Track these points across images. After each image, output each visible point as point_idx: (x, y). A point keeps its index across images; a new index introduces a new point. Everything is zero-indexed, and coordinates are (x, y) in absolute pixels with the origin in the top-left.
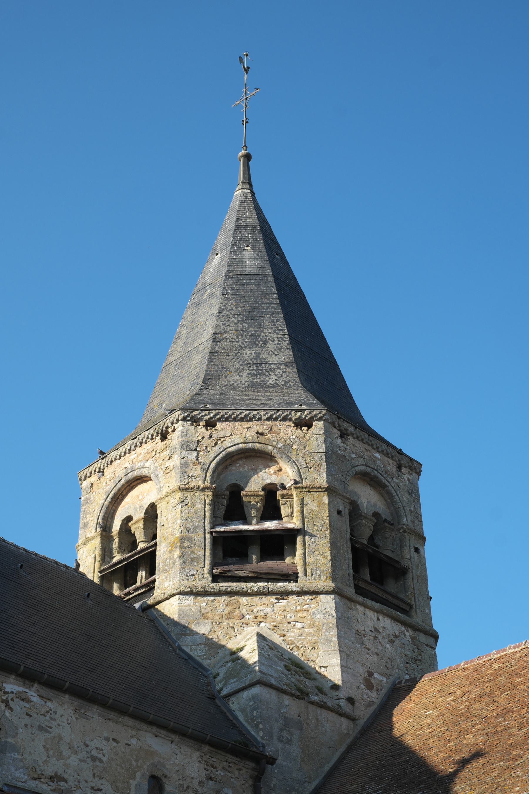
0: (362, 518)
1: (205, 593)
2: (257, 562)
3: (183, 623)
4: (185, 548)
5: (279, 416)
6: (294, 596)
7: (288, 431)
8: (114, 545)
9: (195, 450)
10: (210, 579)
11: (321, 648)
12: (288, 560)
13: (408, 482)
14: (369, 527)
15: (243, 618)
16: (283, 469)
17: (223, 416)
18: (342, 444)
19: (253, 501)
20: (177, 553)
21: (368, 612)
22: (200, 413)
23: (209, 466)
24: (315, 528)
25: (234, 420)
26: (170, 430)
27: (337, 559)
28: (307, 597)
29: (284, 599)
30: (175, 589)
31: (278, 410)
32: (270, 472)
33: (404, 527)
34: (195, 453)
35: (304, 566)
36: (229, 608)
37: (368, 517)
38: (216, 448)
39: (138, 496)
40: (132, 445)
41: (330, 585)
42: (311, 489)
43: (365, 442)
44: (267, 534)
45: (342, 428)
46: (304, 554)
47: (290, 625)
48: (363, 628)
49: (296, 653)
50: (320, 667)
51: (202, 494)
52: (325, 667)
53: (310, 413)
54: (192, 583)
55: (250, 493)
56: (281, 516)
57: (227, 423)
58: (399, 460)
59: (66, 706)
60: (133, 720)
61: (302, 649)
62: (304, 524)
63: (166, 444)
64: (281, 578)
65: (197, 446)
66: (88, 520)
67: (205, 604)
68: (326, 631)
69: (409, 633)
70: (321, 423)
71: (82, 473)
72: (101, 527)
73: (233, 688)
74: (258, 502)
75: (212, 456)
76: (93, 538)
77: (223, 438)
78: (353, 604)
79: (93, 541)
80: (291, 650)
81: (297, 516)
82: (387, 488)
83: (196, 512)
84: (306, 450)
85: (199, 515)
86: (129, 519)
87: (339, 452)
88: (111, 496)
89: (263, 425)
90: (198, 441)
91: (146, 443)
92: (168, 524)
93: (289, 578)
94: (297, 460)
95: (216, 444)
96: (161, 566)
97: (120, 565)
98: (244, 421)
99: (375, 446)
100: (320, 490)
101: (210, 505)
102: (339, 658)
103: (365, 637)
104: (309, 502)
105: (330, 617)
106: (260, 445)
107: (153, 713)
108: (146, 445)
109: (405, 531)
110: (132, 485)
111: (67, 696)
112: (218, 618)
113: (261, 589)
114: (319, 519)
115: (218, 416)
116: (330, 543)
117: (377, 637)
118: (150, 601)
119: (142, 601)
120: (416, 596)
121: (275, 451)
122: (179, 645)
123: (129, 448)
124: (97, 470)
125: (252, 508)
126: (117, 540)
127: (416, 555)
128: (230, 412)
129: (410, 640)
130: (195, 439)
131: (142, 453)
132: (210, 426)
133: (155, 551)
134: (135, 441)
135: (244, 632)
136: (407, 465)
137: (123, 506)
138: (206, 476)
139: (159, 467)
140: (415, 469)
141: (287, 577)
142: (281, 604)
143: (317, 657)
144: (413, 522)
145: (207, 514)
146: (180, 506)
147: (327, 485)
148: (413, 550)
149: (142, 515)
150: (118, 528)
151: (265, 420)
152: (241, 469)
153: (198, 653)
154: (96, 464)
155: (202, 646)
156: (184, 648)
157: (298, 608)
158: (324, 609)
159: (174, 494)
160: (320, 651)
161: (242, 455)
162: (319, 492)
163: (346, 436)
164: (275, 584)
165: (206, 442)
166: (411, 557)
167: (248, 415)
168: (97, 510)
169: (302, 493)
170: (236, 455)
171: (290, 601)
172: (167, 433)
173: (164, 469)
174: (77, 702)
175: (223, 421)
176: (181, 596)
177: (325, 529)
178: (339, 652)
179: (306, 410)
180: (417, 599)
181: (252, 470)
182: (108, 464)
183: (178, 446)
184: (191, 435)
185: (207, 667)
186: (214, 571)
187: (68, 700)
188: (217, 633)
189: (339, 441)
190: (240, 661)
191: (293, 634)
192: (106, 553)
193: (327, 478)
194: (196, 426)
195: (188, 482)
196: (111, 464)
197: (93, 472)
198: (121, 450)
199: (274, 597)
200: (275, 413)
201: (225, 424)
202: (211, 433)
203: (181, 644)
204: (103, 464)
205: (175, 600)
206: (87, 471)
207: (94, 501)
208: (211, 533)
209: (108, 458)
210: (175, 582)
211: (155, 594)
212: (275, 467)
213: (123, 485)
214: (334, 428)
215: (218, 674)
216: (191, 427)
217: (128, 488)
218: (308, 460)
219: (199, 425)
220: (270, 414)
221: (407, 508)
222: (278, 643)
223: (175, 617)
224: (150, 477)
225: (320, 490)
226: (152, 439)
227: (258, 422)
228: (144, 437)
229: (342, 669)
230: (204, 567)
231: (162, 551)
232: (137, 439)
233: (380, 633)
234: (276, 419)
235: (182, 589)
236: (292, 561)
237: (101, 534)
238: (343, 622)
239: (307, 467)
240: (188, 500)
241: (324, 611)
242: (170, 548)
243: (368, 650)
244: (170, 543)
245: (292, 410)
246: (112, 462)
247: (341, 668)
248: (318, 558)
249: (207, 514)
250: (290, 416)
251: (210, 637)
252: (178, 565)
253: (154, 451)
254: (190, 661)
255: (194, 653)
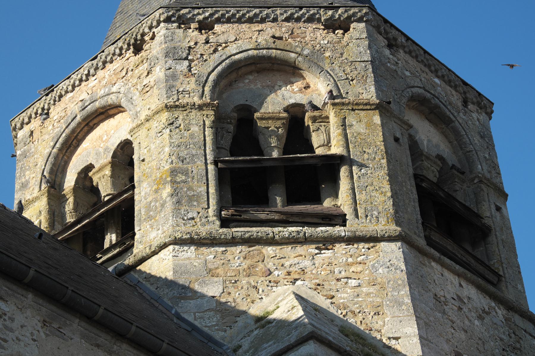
0: (424, 158)
1: (211, 242)
2: (283, 206)
3: (181, 283)
4: (179, 183)
5: (303, 15)
6: (342, 244)
7: (315, 35)
8: (66, 207)
9: (186, 59)
10: (218, 223)
11: (389, 313)
12: (328, 203)
13: (478, 123)
14: (433, 172)
15: (269, 275)
16: (312, 86)
17: (223, 15)
18: (391, 57)
19: (272, 125)
20: (168, 190)
21: (446, 273)
22: (190, 12)
23: (208, 78)
24: (366, 156)
25: (239, 21)
26: (147, 38)
27: (400, 197)
28: (361, 245)
29: (328, 249)
30: (165, 244)
31: (301, 8)
32: (293, 90)
33: (480, 175)
34: (186, 63)
35: (353, 206)
36: (249, 262)
37: (431, 158)
38: (217, 55)
39: (101, 137)
40: (90, 68)
41: (393, 229)
42: (357, 106)
43: (420, 60)
44: (297, 163)
45: (390, 36)
46: (353, 189)
47: (339, 283)
48: (442, 293)
49: (352, 320)
50: (389, 338)
51: (199, 114)
52: (397, 339)
53: (346, 11)
54: (192, 229)
55: (267, 116)
56: (312, 147)
57: (229, 25)
58: (465, 93)
59: (29, 313)
60: (135, 352)
61: (360, 314)
62: (349, 151)
63: (141, 57)
64: (320, 221)
65: (189, 54)
66: (27, 178)
67: (212, 256)
68: (394, 289)
69: (501, 312)
70: (362, 25)
71: (17, 119)
72: (48, 182)
73: (270, 352)
74: (280, 127)
75: (210, 66)
76: (37, 198)
77: (226, 43)
78: (426, 259)
79: (36, 204)
80: (344, 316)
81: (338, 141)
82: (453, 124)
83: (192, 136)
84: (343, 58)
85: (196, 140)
86: (90, 167)
87: (389, 65)
88: (61, 140)
89: (281, 27)
90: (190, 47)
91: (111, 62)
92: (151, 156)
93: (333, 222)
94: (333, 70)
95: (215, 51)
96: (143, 213)
97: (79, 226)
98: (253, 23)
99: (433, 68)
100: (368, 107)
101: (212, 128)
102: (416, 326)
103: (446, 305)
104: (354, 123)
105: (398, 272)
106: (279, 52)
107: (167, 341)
108: (112, 65)
109: (481, 181)
110: (91, 124)
111: (30, 296)
112: (233, 274)
113: (294, 234)
114: (369, 145)
115: (216, 16)
116: (389, 175)
117: (461, 309)
118: (129, 260)
119: (116, 265)
120: (504, 265)
121: (300, 59)
122: (176, 311)
123: (86, 72)
124: (40, 111)
125: (270, 136)
126: (71, 200)
127: (498, 214)
128: (233, 11)
129: (503, 320)
130: (186, 45)
131: (107, 76)
132: (205, 30)
133: (131, 201)
134: (95, 62)
135: (273, 293)
136: (475, 100)
137: (79, 154)
138: (203, 91)
139: (132, 88)
140: (485, 107)
141: (330, 220)
142: (324, 255)
143: (384, 326)
144: (490, 172)
145: (207, 139)
146: (168, 130)
147: (378, 101)
148: (493, 207)
149: (109, 159)
150: (73, 184)
151: (283, 21)
152: (252, 86)
153: (207, 323)
154: (37, 105)
155: (212, 313)
156: (185, 316)
157: (350, 260)
158: (388, 260)
159: (158, 116)
160: (387, 317)
161: (253, 68)
162: (367, 110)
163: (395, 48)
164: (313, 229)
165: (200, 49)
166: (492, 216)
167: (259, 15)
168: (41, 163)
169: (343, 111)
170: (245, 66)
171: (338, 251)
172: (143, 41)
173: (140, 88)
174: (47, 308)
175: (223, 23)
176: (177, 247)
177: (380, 157)
178: (415, 318)
179: (339, 7)
180: (505, 269)
181: (268, 86)
182: (55, 101)
183: (160, 56)
184: (178, 39)
185: (222, 341)
186: (223, 213)
187: (32, 303)
188: (232, 295)
189: (387, 52)
190: (274, 324)
191: (346, 295)
192: (56, 218)
193: (377, 92)
194: (186, 29)
195: (178, 99)
196: (60, 100)
197: (33, 116)
198: (75, 77)
199: (314, 246)
200: (296, 12)
201: (226, 26)
202: (208, 38)
203: (179, 310)
204: (47, 102)
205: (168, 253)
206: (25, 116)
207: (35, 153)
208: (216, 163)
209: (55, 92)
210: (165, 228)
211: (135, 250)
212: (299, 83)
213: (79, 124)
214: (379, 35)
215: (240, 347)
216: (178, 30)
217: (86, 128)
218: (348, 70)
219: (190, 28)
220: (289, 13)
221: (481, 154)
222: (324, 307)
223: (170, 275)
224: (120, 106)
225: (368, 107)
226: (120, 55)
227: (273, 24)
228: (109, 55)
229: (421, 342)
230: (209, 207)
231: (143, 194)
232: (99, 58)
233: (465, 303)
234: (298, 20)
235: (179, 235)
236: (333, 203)
237: (49, 192)
238: (416, 280)
239: (347, 79)
240: (180, 121)
241: (388, 263)
242: (155, 187)
243: (453, 322)
244: (156, 180)
245: (321, 7)
246: (61, 96)
247: (420, 339)
248: (373, 194)
249: (209, 139)
250: (317, 16)
251: (223, 300)
252: (169, 206)
253: (125, 70)
254: (194, 333)
255: (200, 323)
